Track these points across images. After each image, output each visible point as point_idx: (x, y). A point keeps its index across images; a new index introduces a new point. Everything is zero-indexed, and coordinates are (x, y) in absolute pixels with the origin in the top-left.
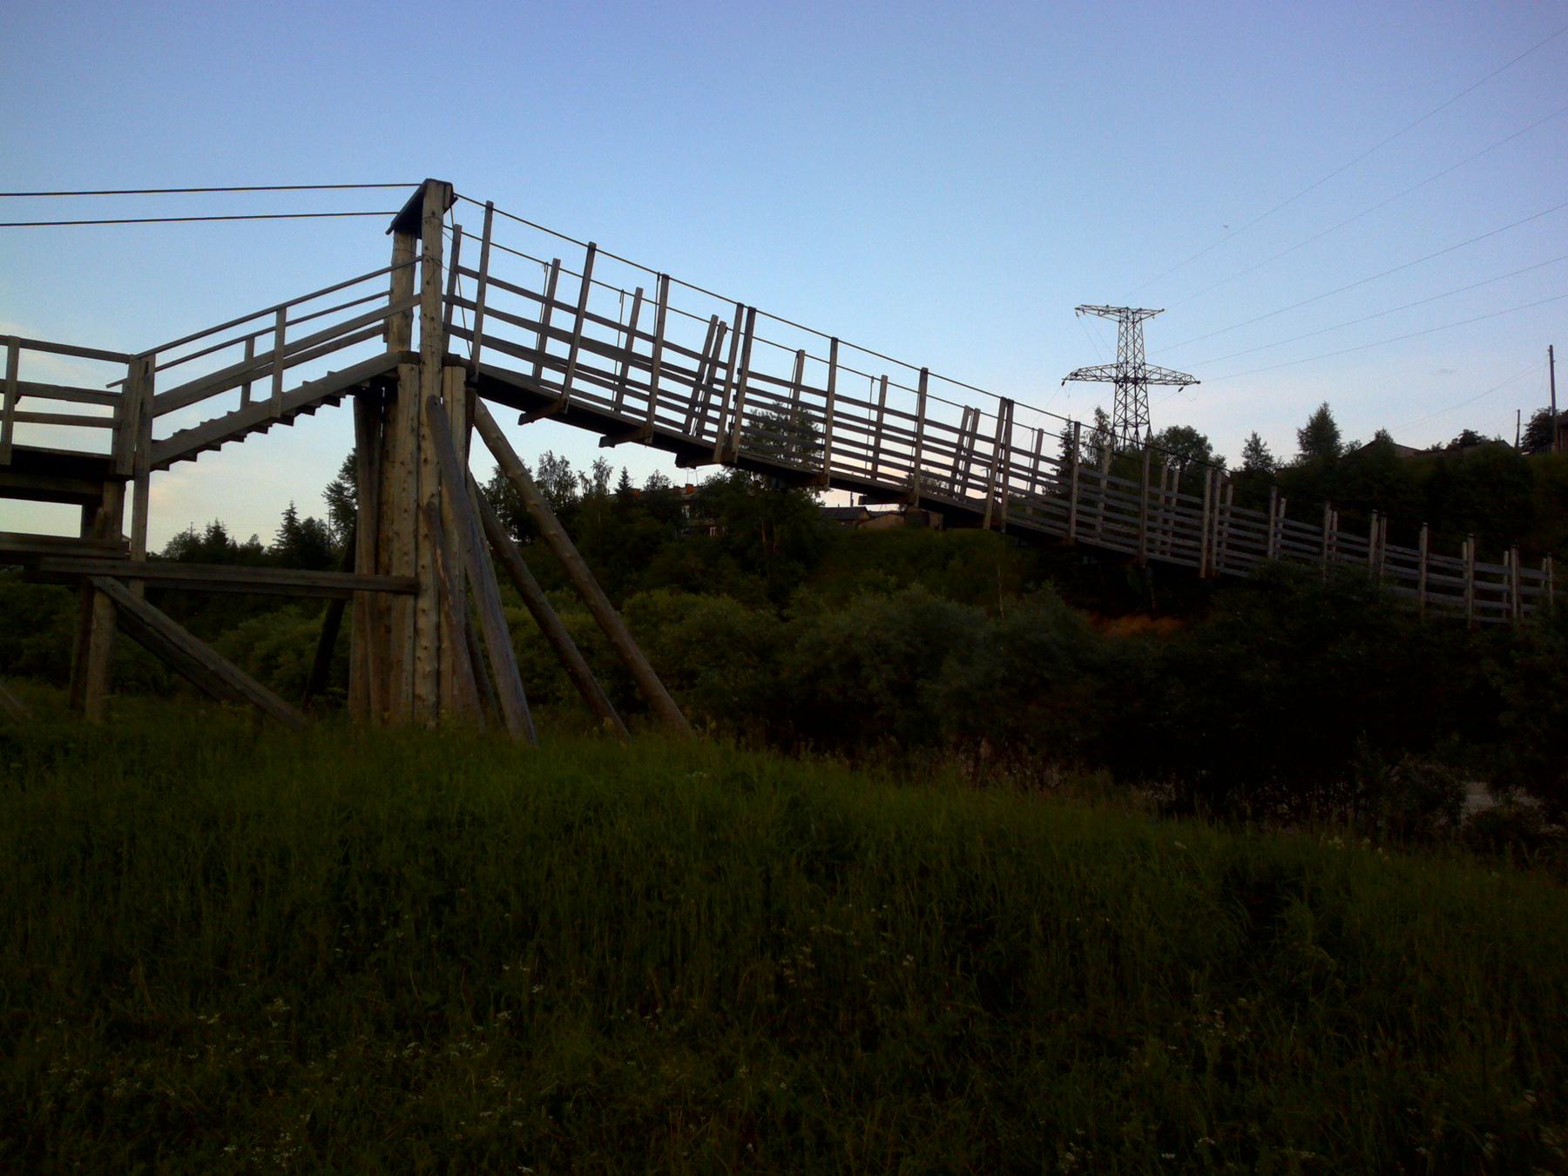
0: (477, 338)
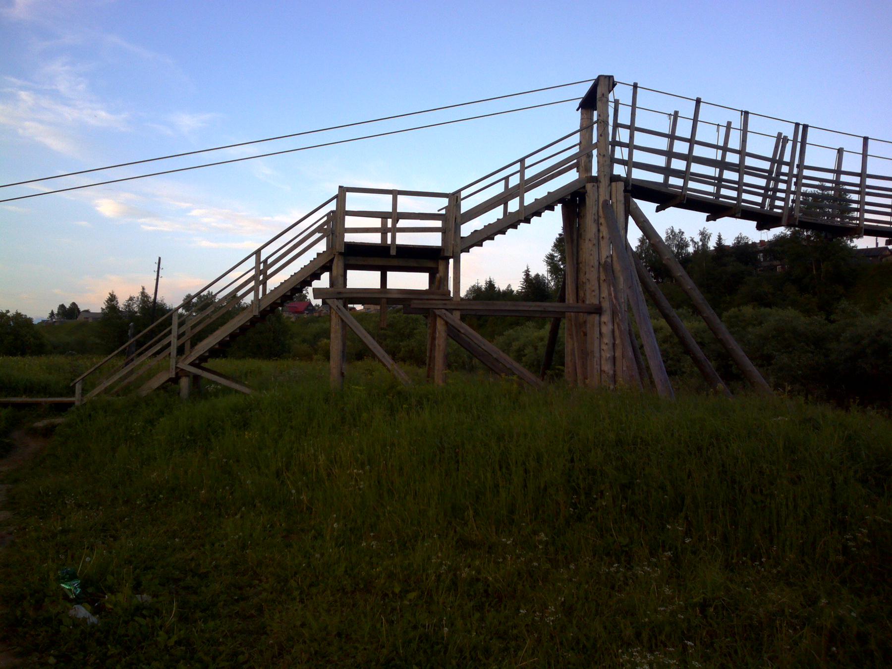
0: (629, 164)
